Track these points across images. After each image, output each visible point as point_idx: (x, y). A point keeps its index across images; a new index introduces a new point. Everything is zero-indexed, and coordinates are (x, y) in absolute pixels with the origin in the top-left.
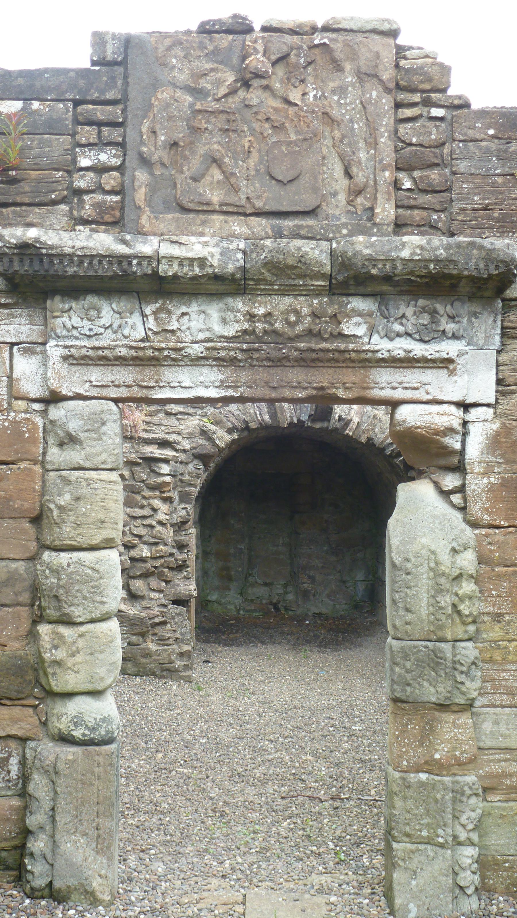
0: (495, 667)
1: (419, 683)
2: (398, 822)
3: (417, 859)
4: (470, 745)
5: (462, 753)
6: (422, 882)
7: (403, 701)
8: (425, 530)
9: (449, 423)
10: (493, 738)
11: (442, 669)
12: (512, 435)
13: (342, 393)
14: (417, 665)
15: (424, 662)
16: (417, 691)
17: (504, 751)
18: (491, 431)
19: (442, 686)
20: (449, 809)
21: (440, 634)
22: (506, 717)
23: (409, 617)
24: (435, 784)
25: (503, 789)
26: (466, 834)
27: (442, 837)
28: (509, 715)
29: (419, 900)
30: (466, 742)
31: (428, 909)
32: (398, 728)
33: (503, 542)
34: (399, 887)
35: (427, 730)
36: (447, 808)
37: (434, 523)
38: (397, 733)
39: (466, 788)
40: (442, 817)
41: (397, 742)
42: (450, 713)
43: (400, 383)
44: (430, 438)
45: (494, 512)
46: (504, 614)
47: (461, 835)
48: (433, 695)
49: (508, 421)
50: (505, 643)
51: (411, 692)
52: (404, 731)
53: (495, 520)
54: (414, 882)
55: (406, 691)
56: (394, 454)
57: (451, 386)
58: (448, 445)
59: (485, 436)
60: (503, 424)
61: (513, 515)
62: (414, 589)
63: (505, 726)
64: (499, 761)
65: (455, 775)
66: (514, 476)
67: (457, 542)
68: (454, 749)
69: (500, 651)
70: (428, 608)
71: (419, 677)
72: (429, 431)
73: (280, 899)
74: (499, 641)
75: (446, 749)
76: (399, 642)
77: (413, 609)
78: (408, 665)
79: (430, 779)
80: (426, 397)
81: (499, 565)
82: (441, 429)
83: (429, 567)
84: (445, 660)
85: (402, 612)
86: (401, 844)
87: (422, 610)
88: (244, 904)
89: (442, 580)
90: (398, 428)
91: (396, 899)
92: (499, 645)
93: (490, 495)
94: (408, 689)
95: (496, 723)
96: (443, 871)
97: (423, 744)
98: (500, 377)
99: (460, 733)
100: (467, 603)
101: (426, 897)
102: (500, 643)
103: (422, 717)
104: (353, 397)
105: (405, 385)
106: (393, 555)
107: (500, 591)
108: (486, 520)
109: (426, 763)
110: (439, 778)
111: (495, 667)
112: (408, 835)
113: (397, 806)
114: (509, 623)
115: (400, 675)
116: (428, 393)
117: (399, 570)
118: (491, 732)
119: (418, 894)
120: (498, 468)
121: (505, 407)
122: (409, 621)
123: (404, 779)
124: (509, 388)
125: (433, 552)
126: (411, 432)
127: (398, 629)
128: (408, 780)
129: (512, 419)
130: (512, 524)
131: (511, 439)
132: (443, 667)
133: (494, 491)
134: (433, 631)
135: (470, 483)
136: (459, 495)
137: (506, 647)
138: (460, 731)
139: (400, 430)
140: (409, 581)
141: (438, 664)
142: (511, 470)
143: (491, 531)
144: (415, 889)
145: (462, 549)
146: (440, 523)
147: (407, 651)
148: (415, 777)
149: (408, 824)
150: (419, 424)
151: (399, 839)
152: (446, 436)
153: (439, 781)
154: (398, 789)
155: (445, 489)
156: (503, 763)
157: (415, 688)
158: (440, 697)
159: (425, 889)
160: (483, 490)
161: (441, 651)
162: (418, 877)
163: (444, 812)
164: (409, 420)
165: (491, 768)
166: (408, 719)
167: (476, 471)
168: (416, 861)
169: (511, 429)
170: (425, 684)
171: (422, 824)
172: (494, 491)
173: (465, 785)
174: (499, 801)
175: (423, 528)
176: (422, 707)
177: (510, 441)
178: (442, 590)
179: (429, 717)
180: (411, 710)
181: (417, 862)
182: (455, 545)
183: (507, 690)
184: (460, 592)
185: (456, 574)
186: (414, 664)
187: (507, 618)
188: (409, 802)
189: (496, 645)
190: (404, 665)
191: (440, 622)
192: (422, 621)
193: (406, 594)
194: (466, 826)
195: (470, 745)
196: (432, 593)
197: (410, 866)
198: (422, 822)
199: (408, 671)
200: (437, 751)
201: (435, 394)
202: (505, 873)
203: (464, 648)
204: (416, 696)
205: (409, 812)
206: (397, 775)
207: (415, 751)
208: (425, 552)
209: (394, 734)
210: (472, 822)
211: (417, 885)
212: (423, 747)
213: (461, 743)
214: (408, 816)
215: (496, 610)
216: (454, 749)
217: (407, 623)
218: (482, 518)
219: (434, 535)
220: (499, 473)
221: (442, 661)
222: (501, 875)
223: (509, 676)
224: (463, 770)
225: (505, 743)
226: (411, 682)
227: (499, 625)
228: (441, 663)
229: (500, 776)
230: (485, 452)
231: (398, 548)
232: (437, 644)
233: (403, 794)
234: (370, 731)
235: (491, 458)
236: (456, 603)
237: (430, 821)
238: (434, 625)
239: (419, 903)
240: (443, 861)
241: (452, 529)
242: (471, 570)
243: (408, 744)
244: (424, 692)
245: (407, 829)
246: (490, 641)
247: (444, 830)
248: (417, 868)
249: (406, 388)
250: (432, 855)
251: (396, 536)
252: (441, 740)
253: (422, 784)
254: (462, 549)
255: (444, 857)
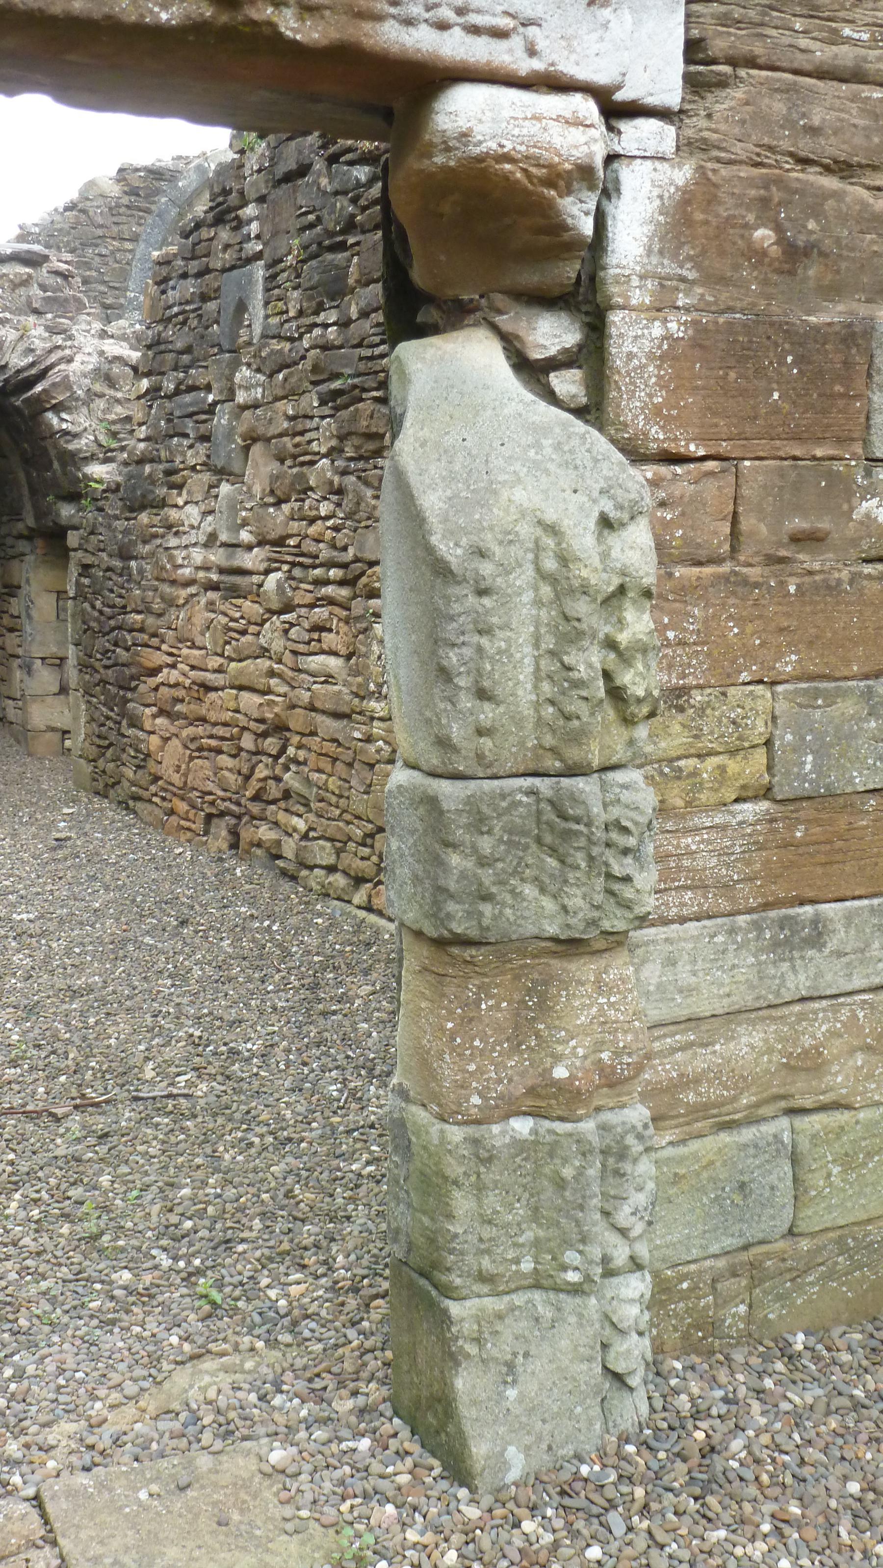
0: (669, 826)
1: (512, 892)
2: (462, 1253)
3: (509, 1330)
4: (636, 1033)
5: (617, 1054)
6: (532, 1388)
7: (466, 942)
8: (517, 466)
9: (584, 148)
10: (661, 1000)
11: (578, 849)
12: (720, 203)
13: (293, 24)
14: (510, 843)
15: (524, 833)
16: (508, 911)
17: (682, 1026)
18: (672, 190)
19: (578, 892)
20: (595, 1201)
21: (573, 754)
22: (691, 946)
23: (488, 714)
24: (557, 1142)
25: (680, 1115)
26: (627, 1249)
27: (576, 1269)
28: (697, 939)
29: (529, 1433)
30: (626, 1027)
31: (550, 1448)
32: (451, 1012)
33: (692, 500)
34: (474, 1413)
35: (529, 1008)
36: (591, 1197)
37: (538, 446)
38: (450, 1025)
39: (630, 1140)
40: (577, 1222)
41: (453, 1050)
42: (586, 958)
43: (461, 11)
44: (529, 193)
45: (675, 418)
46: (691, 688)
47: (615, 1254)
48: (552, 917)
49: (709, 165)
50: (692, 762)
51: (495, 918)
52: (471, 1020)
53: (676, 439)
54: (512, 1393)
55: (481, 914)
56: (9, 388)
57: (595, 36)
58: (569, 221)
59: (658, 202)
60: (700, 169)
61: (716, 425)
62: (500, 634)
63: (688, 968)
64: (673, 1050)
65: (598, 1109)
66: (721, 320)
67: (612, 498)
68: (598, 1047)
69: (682, 784)
70: (536, 687)
71: (515, 873)
72: (534, 170)
73: (143, 1495)
74: (679, 758)
75: (581, 1051)
76: (460, 784)
77: (498, 691)
78: (486, 844)
79: (542, 1131)
80: (525, 66)
81: (682, 561)
82: (567, 166)
83: (538, 570)
84: (588, 825)
85: (466, 702)
86: (468, 1303)
87: (520, 693)
88: (54, 1543)
89: (581, 607)
90: (439, 159)
91: (472, 1443)
92: (680, 769)
93: (667, 370)
94: (487, 909)
95: (671, 962)
96: (582, 1350)
97: (519, 1044)
98: (695, 33)
99: (611, 1005)
100: (640, 666)
101: (544, 1421)
102: (682, 763)
103: (517, 978)
104: (325, 42)
105: (474, 19)
106: (434, 540)
107: (685, 630)
108: (656, 440)
109: (532, 1091)
110: (568, 1127)
111: (669, 826)
112: (483, 1278)
113: (459, 1212)
114: (701, 711)
115: (463, 875)
116: (532, 52)
117: (459, 583)
118: (660, 986)
119: (524, 1419)
120: (687, 295)
121: (703, 123)
122: (489, 724)
123: (476, 1142)
124: (714, 68)
125: (553, 530)
126: (484, 171)
127: (455, 749)
128: (488, 1143)
129: (718, 160)
130: (712, 452)
131: (717, 216)
132: (582, 842)
133: (675, 358)
134: (551, 749)
135: (621, 335)
136: (575, 374)
137: (695, 773)
138: (613, 999)
139: (445, 169)
140: (487, 612)
141: (568, 835)
142: (715, 303)
143: (664, 470)
144: (517, 1410)
145: (626, 516)
146: (558, 447)
147: (485, 809)
148: (503, 1133)
149: (488, 1252)
150: (509, 146)
151: (465, 1292)
152: (569, 192)
153: (570, 1135)
154: (461, 1170)
155: (536, 355)
156: (679, 1056)
157: (504, 904)
158: (572, 921)
159: (541, 1404)
160: (651, 356)
161: (574, 799)
162: (521, 1379)
163: (581, 1208)
164: (480, 131)
165: (657, 1072)
166: (479, 988)
167: (634, 302)
168: (507, 1335)
169: (715, 186)
170: (529, 891)
171: (522, 1245)
172: (675, 358)
173: (627, 1133)
174: (671, 1143)
175: (510, 459)
176: (518, 951)
177: (714, 222)
178: (581, 634)
179: (536, 976)
180: (490, 962)
181: (510, 1339)
182: (608, 506)
183: (693, 879)
184: (623, 638)
185: (611, 589)
186: (500, 841)
187: (698, 697)
188: (492, 1199)
189: (673, 770)
190: (474, 848)
191: (576, 723)
192: (518, 721)
193: (480, 649)
194: (628, 1229)
195: (636, 1033)
196: (549, 643)
197: (495, 1352)
198: (521, 1240)
199: (483, 862)
200: (557, 1058)
201: (554, 57)
202: (681, 1305)
203: (625, 786)
204: (506, 925)
205: (490, 1222)
206: (456, 1134)
207: (499, 1066)
208: (526, 530)
209: (442, 1029)
210: (642, 1218)
211: (521, 1399)
212: (521, 1053)
213: (616, 1030)
214: (487, 1232)
215: (674, 681)
216: (598, 1047)
217: (481, 732)
218: (646, 434)
219: (544, 479)
220: (687, 310)
221: (581, 827)
222: (674, 1310)
223: (699, 842)
224: (619, 1095)
225: (689, 1006)
226: (494, 890)
227: (680, 717)
228: (577, 833)
229: (676, 1086)
230: (656, 247)
231: (446, 520)
232: (565, 782)
233: (473, 1178)
234: (51, 919)
235: (669, 268)
236: (611, 667)
237: (541, 1233)
238: (554, 731)
239: (528, 1440)
240: (580, 1325)
241: (596, 461)
242: (647, 574)
243: (482, 1051)
244: (526, 913)
245: (486, 1263)
246: (659, 761)
247: (581, 1252)
248: (515, 1354)
249: (475, 30)
250: (549, 1315)
251: (433, 487)
252: (567, 1031)
253: (520, 1146)
254: (626, 516)
255: (580, 1316)
